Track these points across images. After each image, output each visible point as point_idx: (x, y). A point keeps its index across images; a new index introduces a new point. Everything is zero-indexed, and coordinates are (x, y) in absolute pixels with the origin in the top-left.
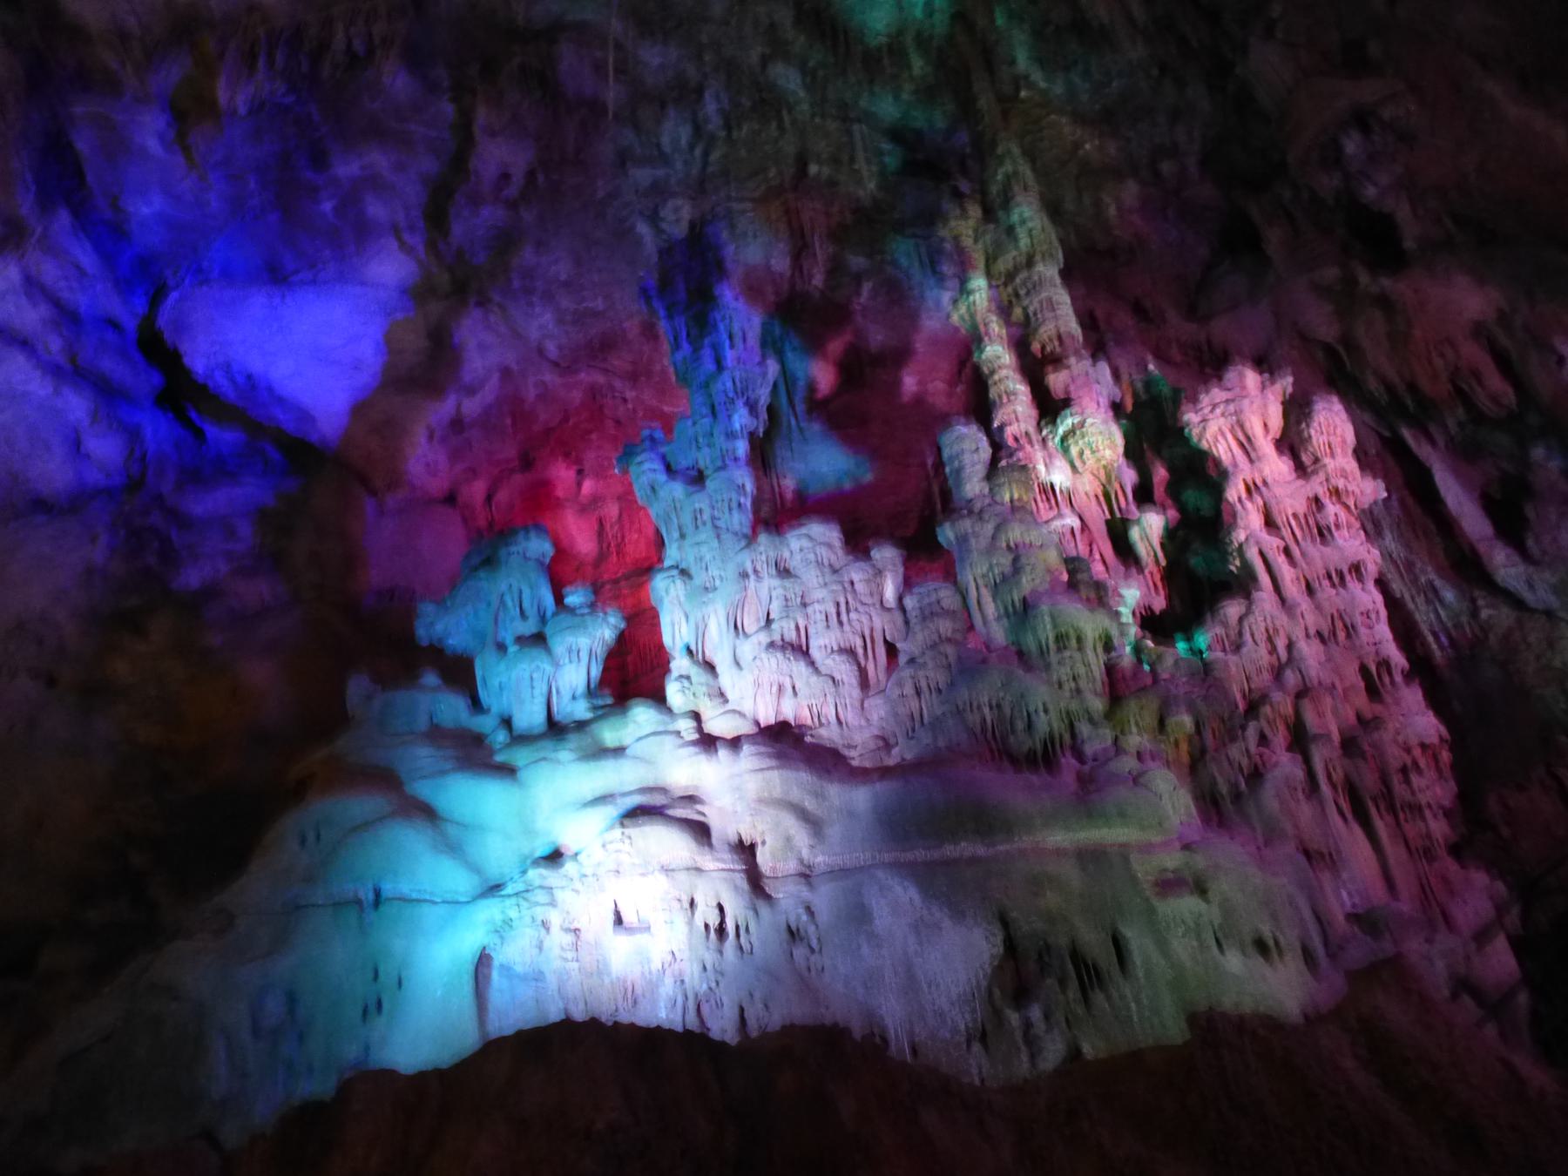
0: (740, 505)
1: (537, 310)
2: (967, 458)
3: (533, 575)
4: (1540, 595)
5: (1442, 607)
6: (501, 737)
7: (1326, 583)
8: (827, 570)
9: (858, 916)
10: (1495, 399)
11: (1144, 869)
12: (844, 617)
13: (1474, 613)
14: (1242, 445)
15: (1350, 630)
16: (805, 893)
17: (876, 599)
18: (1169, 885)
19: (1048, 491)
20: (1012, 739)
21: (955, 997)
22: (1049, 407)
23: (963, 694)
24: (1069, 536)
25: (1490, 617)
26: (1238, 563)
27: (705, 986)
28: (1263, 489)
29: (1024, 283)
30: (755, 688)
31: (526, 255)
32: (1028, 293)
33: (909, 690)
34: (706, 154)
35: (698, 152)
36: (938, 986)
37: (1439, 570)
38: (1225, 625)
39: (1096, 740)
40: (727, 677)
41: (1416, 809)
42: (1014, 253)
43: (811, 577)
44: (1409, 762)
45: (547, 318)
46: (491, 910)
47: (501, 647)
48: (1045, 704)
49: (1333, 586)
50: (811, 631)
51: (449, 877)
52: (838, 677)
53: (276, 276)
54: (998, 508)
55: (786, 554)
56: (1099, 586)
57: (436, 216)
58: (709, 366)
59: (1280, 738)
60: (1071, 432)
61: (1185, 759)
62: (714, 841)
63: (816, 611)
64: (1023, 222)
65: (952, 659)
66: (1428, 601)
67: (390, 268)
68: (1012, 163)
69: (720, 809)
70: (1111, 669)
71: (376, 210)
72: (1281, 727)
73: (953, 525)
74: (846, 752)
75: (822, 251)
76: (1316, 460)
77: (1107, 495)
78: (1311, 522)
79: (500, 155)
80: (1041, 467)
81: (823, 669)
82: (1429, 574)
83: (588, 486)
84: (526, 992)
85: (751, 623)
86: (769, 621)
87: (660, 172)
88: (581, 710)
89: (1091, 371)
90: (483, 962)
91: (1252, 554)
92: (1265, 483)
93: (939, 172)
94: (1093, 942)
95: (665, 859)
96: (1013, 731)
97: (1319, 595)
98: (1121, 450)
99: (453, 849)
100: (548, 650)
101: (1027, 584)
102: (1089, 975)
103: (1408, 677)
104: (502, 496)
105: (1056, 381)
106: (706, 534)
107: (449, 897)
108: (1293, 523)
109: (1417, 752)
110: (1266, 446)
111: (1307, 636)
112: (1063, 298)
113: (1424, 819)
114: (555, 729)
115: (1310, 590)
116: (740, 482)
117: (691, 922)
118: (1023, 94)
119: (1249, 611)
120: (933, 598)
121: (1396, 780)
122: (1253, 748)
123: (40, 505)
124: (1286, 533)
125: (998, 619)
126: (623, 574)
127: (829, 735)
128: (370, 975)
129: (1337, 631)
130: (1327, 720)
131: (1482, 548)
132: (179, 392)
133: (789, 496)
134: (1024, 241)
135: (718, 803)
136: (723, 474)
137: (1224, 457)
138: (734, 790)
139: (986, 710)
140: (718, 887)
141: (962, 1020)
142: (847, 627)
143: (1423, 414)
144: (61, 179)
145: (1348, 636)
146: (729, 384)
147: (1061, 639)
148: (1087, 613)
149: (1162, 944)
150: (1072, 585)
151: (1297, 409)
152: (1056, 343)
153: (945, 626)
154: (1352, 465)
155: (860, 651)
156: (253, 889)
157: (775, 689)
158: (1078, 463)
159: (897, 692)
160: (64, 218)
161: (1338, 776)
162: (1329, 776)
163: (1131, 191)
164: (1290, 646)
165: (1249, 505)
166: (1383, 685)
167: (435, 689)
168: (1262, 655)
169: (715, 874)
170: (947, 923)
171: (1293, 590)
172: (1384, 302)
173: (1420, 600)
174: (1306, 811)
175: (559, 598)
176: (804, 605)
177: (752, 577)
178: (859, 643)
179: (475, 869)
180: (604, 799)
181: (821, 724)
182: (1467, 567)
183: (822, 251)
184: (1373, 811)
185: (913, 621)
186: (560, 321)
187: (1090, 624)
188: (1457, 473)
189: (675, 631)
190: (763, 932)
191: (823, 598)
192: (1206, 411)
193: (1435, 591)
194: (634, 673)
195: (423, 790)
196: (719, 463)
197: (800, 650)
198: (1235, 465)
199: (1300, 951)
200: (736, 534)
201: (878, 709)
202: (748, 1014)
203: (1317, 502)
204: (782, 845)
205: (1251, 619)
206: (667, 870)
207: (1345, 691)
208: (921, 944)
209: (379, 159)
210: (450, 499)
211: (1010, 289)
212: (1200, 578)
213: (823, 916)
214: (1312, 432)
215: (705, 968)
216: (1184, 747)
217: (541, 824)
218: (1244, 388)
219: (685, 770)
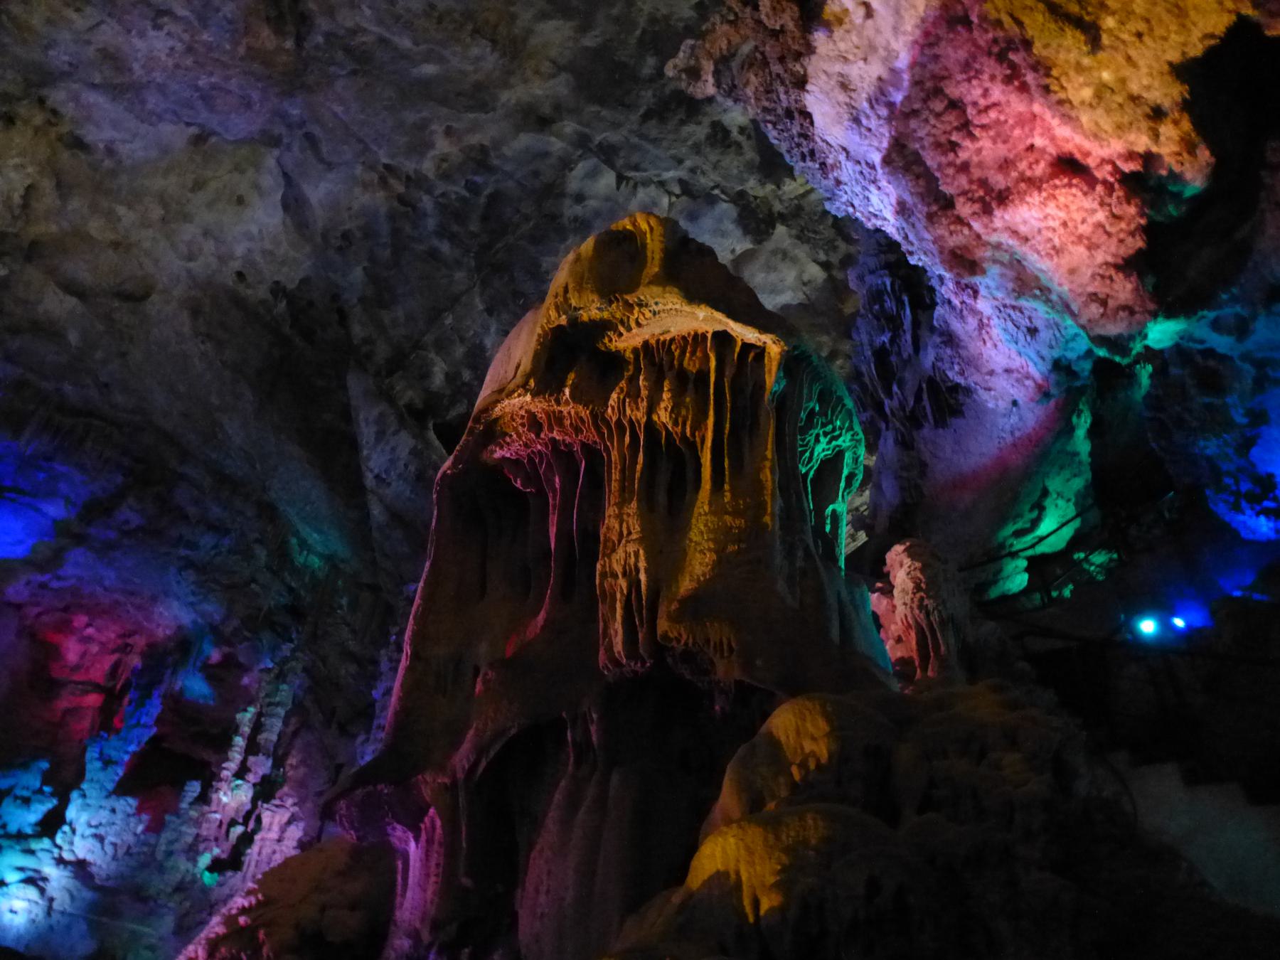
9: (68, 927)
30: (82, 848)
34: (216, 555)
35: (213, 553)
40: (77, 839)
75: (235, 623)
83: (90, 630)
88: (29, 831)
101: (177, 846)
104: (45, 618)
126: (64, 783)
127: (94, 870)
138: (57, 877)
140: (39, 912)
153: (145, 849)
156: (21, 949)
163: (353, 668)
180: (21, 869)
189: (71, 813)
206: (29, 900)
210: (19, 607)
219: (50, 870)
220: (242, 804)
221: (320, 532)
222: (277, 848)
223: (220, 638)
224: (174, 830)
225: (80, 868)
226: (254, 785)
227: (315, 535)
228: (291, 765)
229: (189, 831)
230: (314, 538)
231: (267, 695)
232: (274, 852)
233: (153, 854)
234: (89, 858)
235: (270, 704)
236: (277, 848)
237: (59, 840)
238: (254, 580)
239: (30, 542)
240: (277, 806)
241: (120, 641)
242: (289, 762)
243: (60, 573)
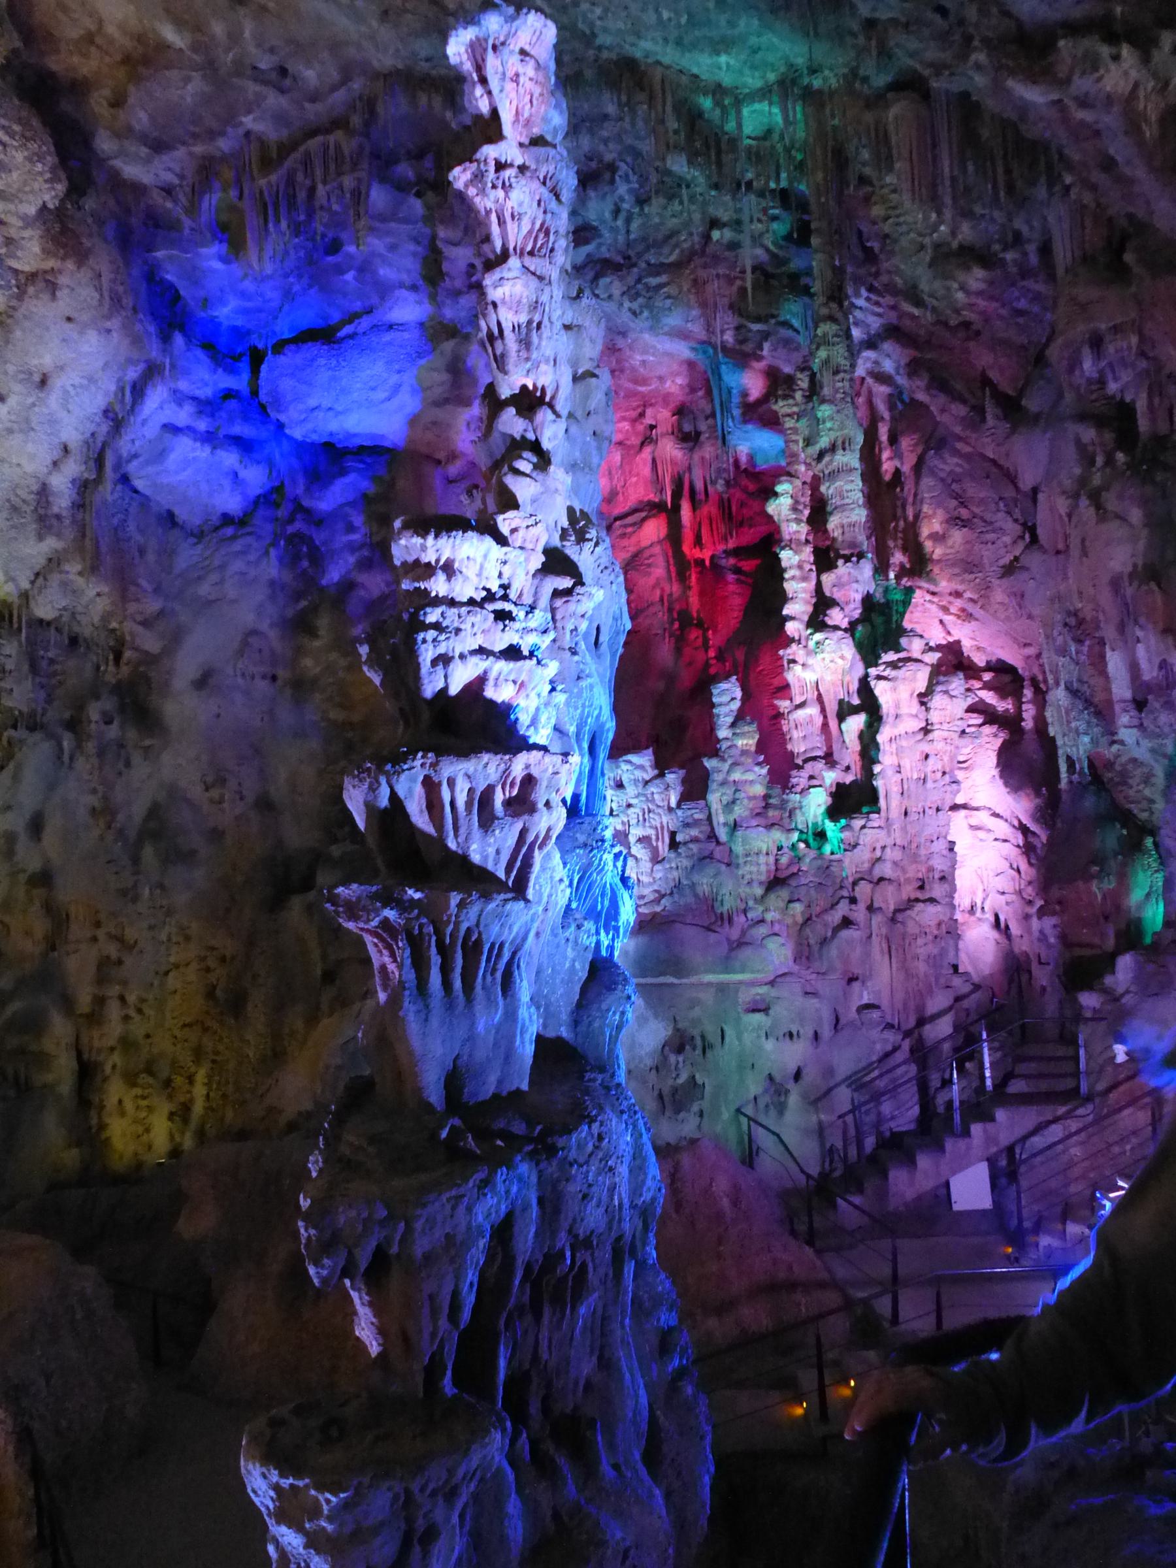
23: (696, 878)
34: (628, 220)
35: (620, 223)
71: (385, 272)
141: (649, 1062)
149: (739, 1038)
160: (179, 340)
161: (884, 931)
163: (977, 278)
170: (651, 1018)
221: (721, 45)
222: (926, 747)
223: (742, 357)
224: (724, 783)
226: (851, 629)
227: (723, 59)
228: (934, 537)
229: (750, 776)
230: (720, 67)
231: (808, 442)
233: (712, 836)
235: (821, 455)
236: (926, 747)
238: (714, 223)
239: (408, 378)
240: (894, 665)
241: (640, 428)
242: (925, 531)
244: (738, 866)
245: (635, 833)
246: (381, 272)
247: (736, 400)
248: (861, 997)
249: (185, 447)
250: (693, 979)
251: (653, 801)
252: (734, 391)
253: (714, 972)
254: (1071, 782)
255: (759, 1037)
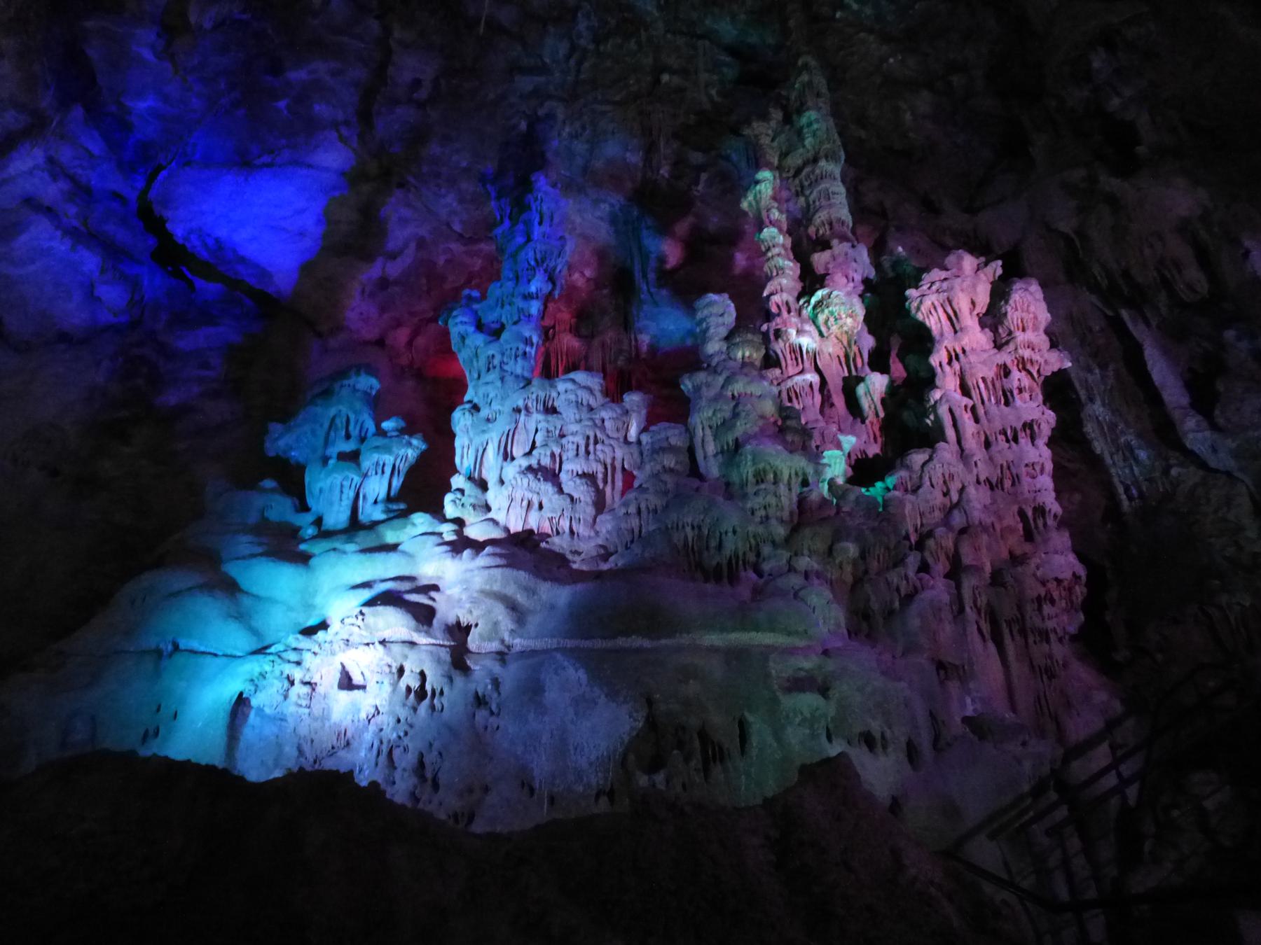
0: (525, 353)
1: (443, 191)
2: (713, 321)
3: (358, 405)
4: (1222, 460)
5: (1130, 465)
6: (311, 531)
7: (1001, 438)
8: (585, 409)
9: (533, 690)
10: (1191, 287)
11: (779, 669)
12: (591, 448)
13: (1166, 471)
14: (950, 318)
15: (1016, 480)
16: (497, 668)
17: (621, 435)
18: (798, 684)
19: (797, 351)
20: (706, 554)
21: (593, 758)
22: (811, 281)
23: (674, 516)
24: (807, 389)
25: (1179, 474)
26: (932, 417)
27: (395, 735)
28: (961, 356)
29: (808, 176)
30: (511, 504)
31: (434, 148)
32: (810, 185)
33: (632, 509)
34: (580, 63)
35: (572, 62)
36: (582, 750)
37: (1139, 435)
38: (909, 468)
39: (774, 561)
40: (495, 496)
41: (1044, 635)
42: (801, 150)
43: (569, 413)
44: (1043, 594)
45: (450, 199)
46: (254, 666)
47: (325, 460)
48: (733, 528)
49: (1008, 441)
50: (564, 458)
51: (235, 638)
52: (576, 496)
53: (243, 163)
54: (731, 363)
55: (554, 394)
56: (806, 433)
57: (365, 116)
58: (520, 240)
59: (941, 567)
60: (819, 304)
61: (849, 579)
62: (435, 621)
63: (570, 442)
64: (810, 124)
65: (670, 486)
66: (1125, 459)
67: (333, 157)
68: (810, 75)
69: (449, 597)
70: (802, 501)
71: (321, 109)
72: (943, 557)
73: (690, 378)
74: (570, 557)
75: (666, 149)
76: (1010, 333)
77: (847, 356)
78: (998, 385)
79: (412, 67)
80: (793, 332)
81: (566, 490)
82: (1130, 438)
84: (270, 730)
85: (518, 451)
86: (533, 447)
87: (542, 79)
88: (378, 515)
89: (850, 251)
90: (241, 702)
91: (943, 411)
92: (964, 351)
93: (761, 82)
94: (718, 720)
95: (387, 634)
96: (708, 548)
97: (994, 448)
98: (861, 318)
99: (241, 617)
100: (358, 465)
101: (741, 428)
102: (713, 754)
103: (1062, 523)
105: (820, 260)
106: (493, 376)
107: (229, 652)
108: (982, 386)
109: (1052, 585)
110: (970, 321)
111: (978, 482)
112: (840, 189)
113: (1048, 641)
114: (355, 525)
115: (988, 444)
116: (527, 334)
117: (395, 686)
118: (838, 15)
119: (931, 459)
120: (663, 435)
121: (1030, 608)
122: (911, 574)
123: (64, 337)
124: (974, 394)
125: (715, 456)
126: (429, 403)
127: (560, 544)
128: (155, 708)
129: (1003, 482)
130: (983, 556)
131: (1177, 415)
132: (170, 255)
133: (644, 348)
134: (809, 141)
135: (448, 592)
136: (515, 328)
137: (934, 328)
138: (459, 583)
139: (688, 529)
140: (424, 659)
142: (592, 457)
143: (1138, 300)
144: (77, 83)
145: (1013, 484)
146: (531, 254)
147: (760, 478)
148: (785, 454)
149: (778, 735)
150: (782, 431)
151: (1000, 292)
152: (827, 227)
153: (669, 461)
154: (1042, 340)
155: (600, 476)
157: (525, 503)
158: (823, 329)
159: (623, 511)
160: (77, 112)
161: (982, 601)
162: (975, 602)
163: (924, 101)
164: (962, 491)
165: (947, 368)
166: (1037, 527)
167: (273, 490)
168: (938, 499)
169: (424, 648)
171: (972, 444)
172: (1113, 201)
173: (1118, 458)
174: (947, 630)
175: (378, 426)
176: (562, 436)
177: (523, 412)
178: (600, 469)
179: (255, 633)
181: (558, 533)
182: (1164, 433)
183: (666, 149)
184: (1006, 631)
185: (645, 453)
186: (461, 201)
187: (787, 464)
188: (1166, 352)
190: (453, 698)
191: (576, 429)
192: (925, 287)
193: (1132, 451)
194: (424, 489)
195: (233, 569)
196: (515, 319)
197: (550, 475)
198: (942, 335)
199: (904, 746)
200: (517, 377)
201: (606, 524)
202: (427, 760)
203: (1005, 371)
204: (490, 630)
205: (931, 465)
207: (1002, 530)
208: (576, 714)
209: (321, 68)
210: (380, 343)
211: (797, 181)
212: (908, 426)
213: (506, 687)
214: (1009, 309)
215: (399, 721)
216: (848, 569)
217: (318, 600)
218: (960, 269)
220: (852, 340)
225: (521, 549)
232: (1005, 371)
234: (535, 521)
237: (450, 510)
243: (391, 245)
244: (745, 496)
245: (572, 466)
246: (317, 108)
247: (653, 264)
248: (963, 706)
249: (40, 232)
250: (685, 639)
251: (603, 428)
252: (653, 256)
253: (723, 630)
254: (1130, 506)
255: (814, 736)
